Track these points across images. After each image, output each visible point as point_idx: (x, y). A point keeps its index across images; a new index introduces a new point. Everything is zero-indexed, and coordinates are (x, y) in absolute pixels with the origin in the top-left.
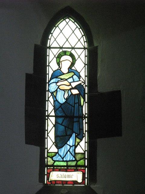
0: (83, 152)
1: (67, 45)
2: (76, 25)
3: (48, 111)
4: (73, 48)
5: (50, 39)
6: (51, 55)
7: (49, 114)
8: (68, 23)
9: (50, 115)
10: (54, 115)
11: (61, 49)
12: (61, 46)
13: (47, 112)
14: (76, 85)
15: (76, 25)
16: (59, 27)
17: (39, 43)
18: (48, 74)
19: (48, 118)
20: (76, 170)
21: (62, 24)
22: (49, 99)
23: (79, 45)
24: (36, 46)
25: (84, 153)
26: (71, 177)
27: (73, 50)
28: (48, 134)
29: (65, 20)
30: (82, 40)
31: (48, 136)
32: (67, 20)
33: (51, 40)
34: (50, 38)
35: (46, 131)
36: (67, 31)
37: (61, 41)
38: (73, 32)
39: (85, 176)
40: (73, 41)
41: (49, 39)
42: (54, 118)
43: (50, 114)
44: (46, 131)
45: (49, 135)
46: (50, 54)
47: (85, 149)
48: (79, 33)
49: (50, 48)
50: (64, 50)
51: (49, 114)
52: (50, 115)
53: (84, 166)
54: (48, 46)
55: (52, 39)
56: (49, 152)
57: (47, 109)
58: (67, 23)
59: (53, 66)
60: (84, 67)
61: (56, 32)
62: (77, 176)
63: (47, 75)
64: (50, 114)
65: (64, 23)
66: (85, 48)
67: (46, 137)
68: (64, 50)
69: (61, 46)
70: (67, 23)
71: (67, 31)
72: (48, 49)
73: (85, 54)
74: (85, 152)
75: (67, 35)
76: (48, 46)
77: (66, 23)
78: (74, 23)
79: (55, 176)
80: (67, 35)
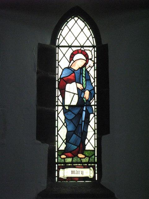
0: (93, 149)
1: (76, 44)
2: (92, 57)
3: (57, 127)
4: (83, 47)
5: (59, 39)
8: (77, 22)
12: (70, 45)
15: (92, 57)
16: (67, 91)
17: (48, 42)
18: (58, 74)
20: (88, 167)
21: (71, 22)
23: (88, 43)
25: (94, 150)
27: (82, 45)
29: (73, 18)
30: (91, 39)
31: (58, 65)
32: (76, 18)
33: (60, 40)
34: (58, 38)
36: (76, 30)
37: (70, 40)
38: (82, 30)
39: (95, 179)
40: (82, 40)
41: (58, 39)
43: (60, 44)
45: (59, 115)
46: (58, 139)
47: (95, 145)
48: (87, 32)
49: (59, 46)
52: (60, 45)
54: (57, 45)
55: (61, 38)
56: (59, 149)
57: (56, 126)
58: (76, 22)
59: (63, 63)
60: (94, 135)
61: (65, 31)
62: (88, 173)
63: (58, 40)
64: (60, 44)
66: (93, 47)
67: (57, 66)
69: (70, 45)
70: (76, 22)
71: (76, 30)
73: (95, 121)
74: (95, 149)
75: (76, 34)
79: (65, 173)
80: (76, 34)
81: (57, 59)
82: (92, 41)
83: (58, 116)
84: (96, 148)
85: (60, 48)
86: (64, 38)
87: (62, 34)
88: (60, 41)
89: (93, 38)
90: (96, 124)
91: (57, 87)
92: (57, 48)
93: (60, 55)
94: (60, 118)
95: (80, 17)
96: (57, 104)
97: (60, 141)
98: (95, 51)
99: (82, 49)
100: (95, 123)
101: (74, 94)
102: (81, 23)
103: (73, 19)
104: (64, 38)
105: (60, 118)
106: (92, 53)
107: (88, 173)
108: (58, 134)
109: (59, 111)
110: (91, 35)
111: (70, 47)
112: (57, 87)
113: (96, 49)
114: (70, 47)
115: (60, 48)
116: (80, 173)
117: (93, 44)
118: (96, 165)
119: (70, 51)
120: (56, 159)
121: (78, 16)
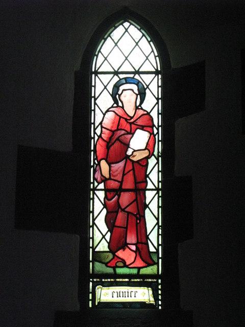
0: (155, 251)
1: (127, 68)
2: (152, 48)
3: (93, 212)
6: (102, 88)
7: (97, 69)
9: (97, 188)
10: (103, 188)
11: (116, 76)
12: (116, 70)
13: (91, 214)
14: (148, 167)
15: (152, 48)
16: (149, 208)
19: (94, 193)
21: (118, 32)
22: (95, 222)
23: (148, 67)
24: (76, 73)
26: (129, 295)
28: (94, 220)
29: (122, 24)
30: (152, 58)
31: (95, 104)
32: (126, 24)
35: (92, 125)
36: (127, 44)
38: (137, 44)
40: (137, 60)
42: (103, 192)
44: (92, 125)
45: (97, 101)
50: (122, 76)
51: (97, 69)
53: (156, 276)
54: (93, 70)
55: (100, 59)
58: (126, 30)
61: (107, 47)
62: (143, 295)
65: (119, 30)
66: (156, 73)
68: (122, 76)
70: (126, 30)
72: (93, 75)
75: (127, 51)
76: (93, 70)
77: (125, 30)
78: (149, 42)
79: (106, 294)
80: (127, 51)
81: (93, 95)
82: (153, 63)
83: (95, 104)
84: (160, 247)
85: (99, 75)
86: (106, 59)
87: (101, 50)
88: (99, 62)
89: (155, 57)
90: (160, 209)
91: (91, 259)
92: (93, 75)
93: (99, 87)
94: (98, 106)
95: (134, 23)
96: (92, 187)
97: (98, 236)
98: (160, 114)
99: (137, 77)
100: (158, 87)
101: (121, 182)
102: (135, 32)
103: (121, 26)
104: (106, 59)
105: (98, 106)
106: (154, 85)
107: (143, 295)
108: (94, 223)
109: (96, 125)
110: (153, 51)
111: (116, 73)
112: (91, 259)
113: (161, 287)
114: (116, 73)
115: (99, 75)
116: (133, 294)
117: (156, 68)
118: (160, 281)
119: (116, 79)
120: (90, 302)
121: (130, 21)
